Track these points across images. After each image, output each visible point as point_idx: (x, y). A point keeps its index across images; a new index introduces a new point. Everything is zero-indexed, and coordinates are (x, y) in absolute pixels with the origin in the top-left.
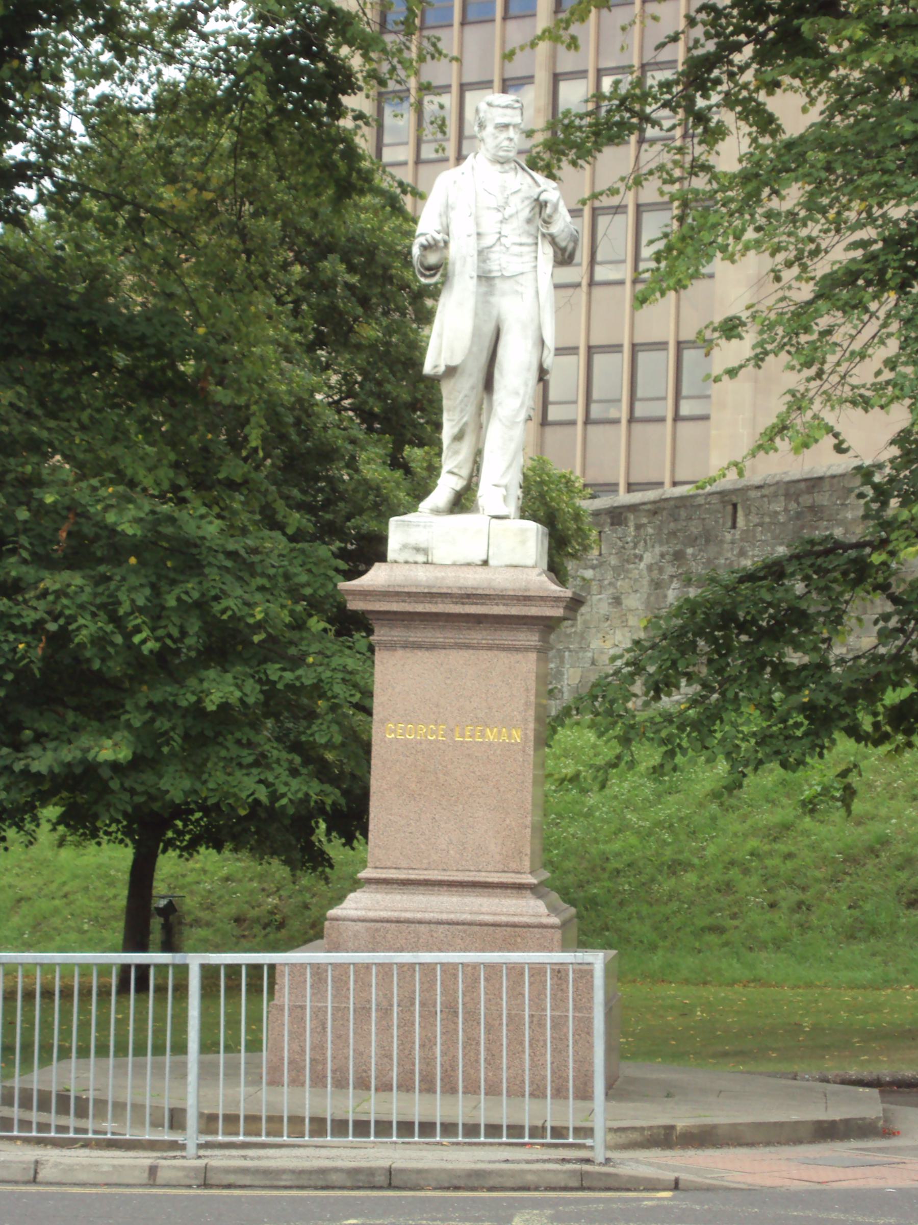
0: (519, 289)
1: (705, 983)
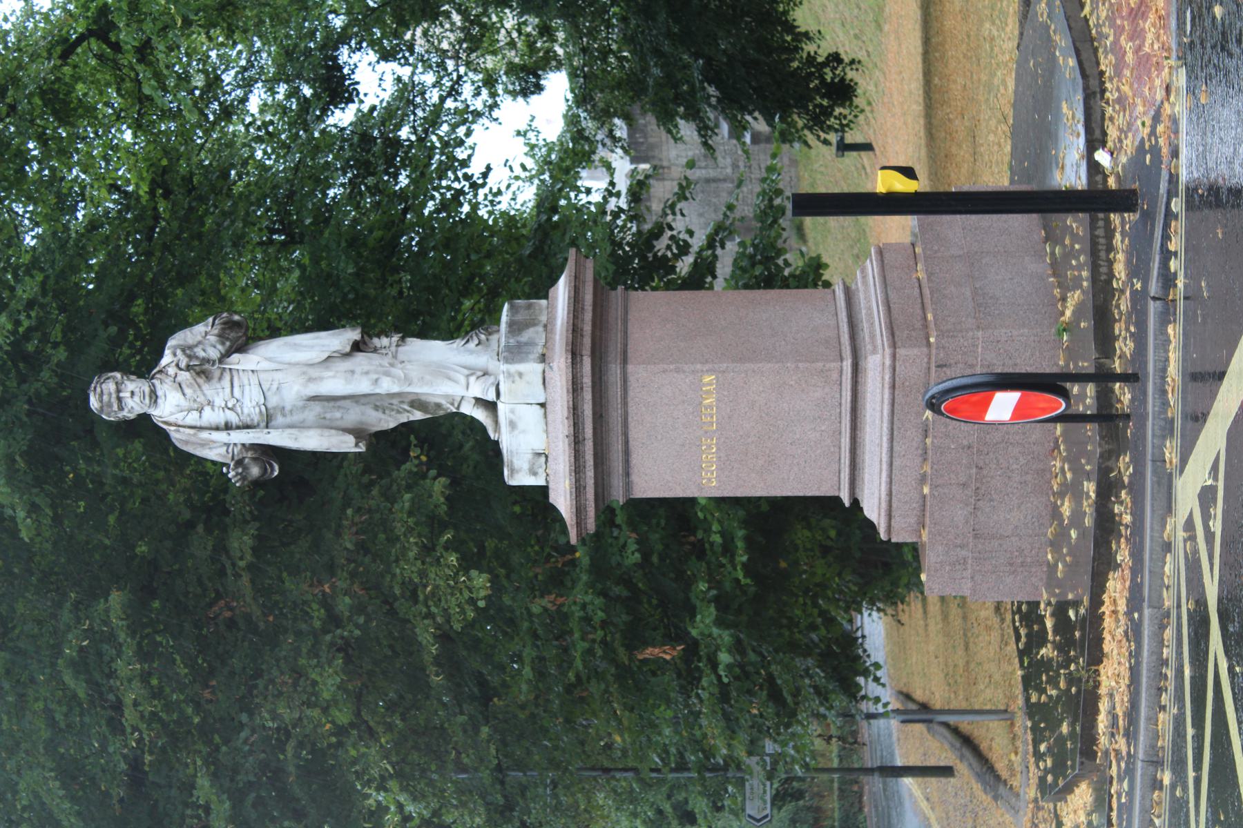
0: (275, 387)
1: (928, 799)
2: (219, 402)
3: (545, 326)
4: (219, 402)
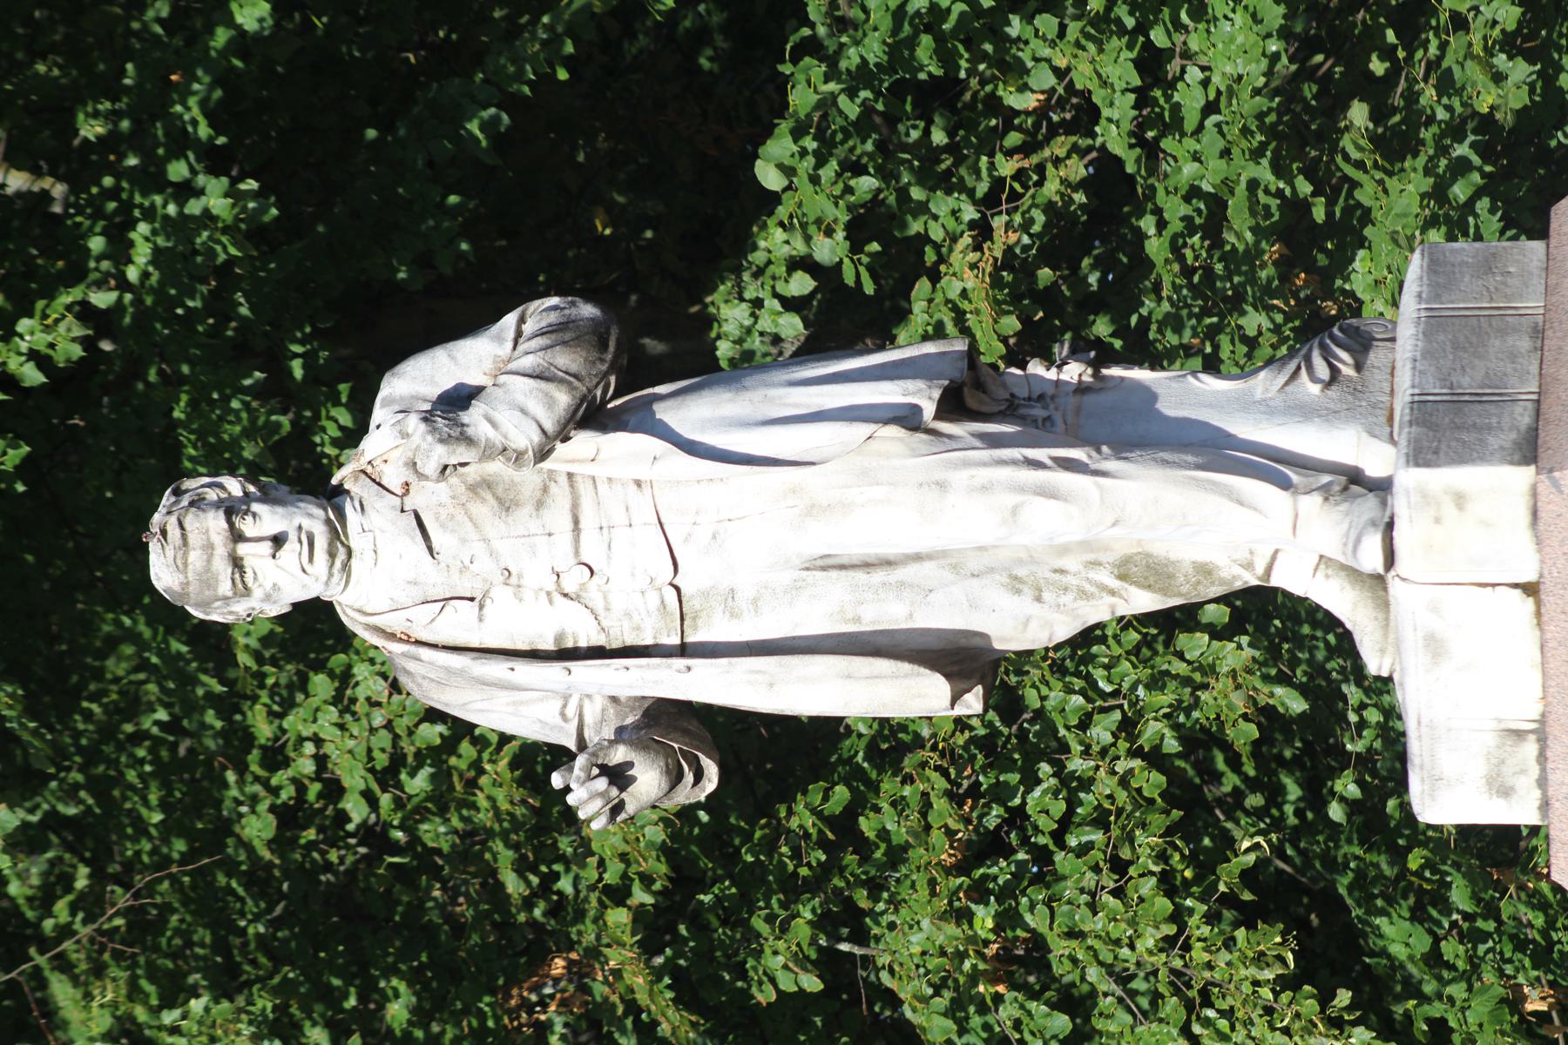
2: (537, 576)
3: (1538, 333)
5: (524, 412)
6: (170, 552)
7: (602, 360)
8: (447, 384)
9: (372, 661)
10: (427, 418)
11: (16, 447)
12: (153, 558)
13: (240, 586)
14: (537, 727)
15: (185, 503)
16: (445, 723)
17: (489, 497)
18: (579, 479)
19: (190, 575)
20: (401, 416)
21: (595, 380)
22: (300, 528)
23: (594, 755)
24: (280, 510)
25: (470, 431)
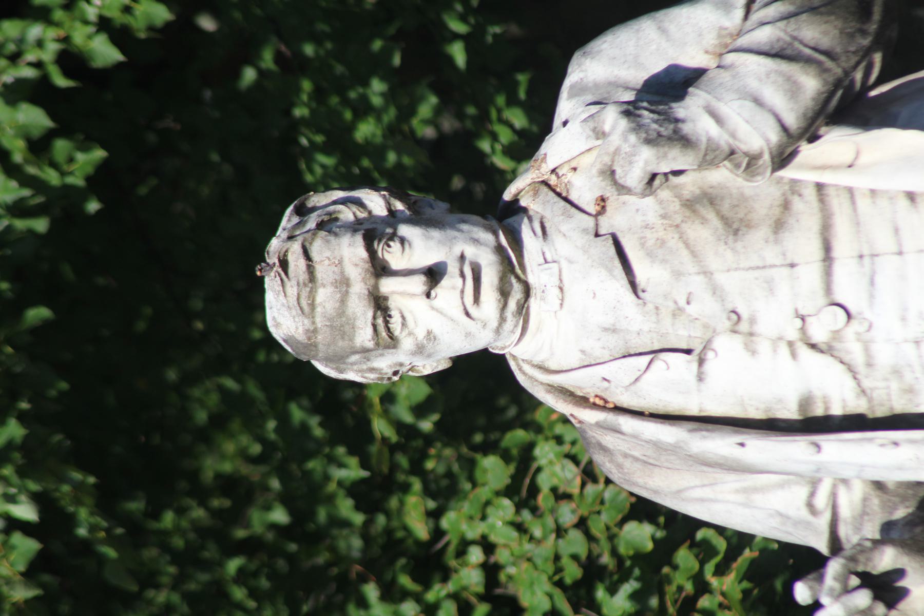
2: (774, 319)
4: (774, 319)
5: (758, 102)
6: (292, 290)
7: (863, 33)
8: (657, 66)
9: (559, 440)
10: (630, 111)
11: (84, 149)
12: (269, 297)
13: (384, 334)
14: (775, 522)
15: (311, 224)
16: (652, 520)
17: (711, 215)
18: (831, 192)
19: (319, 320)
20: (594, 109)
21: (854, 59)
22: (462, 257)
23: (852, 559)
24: (435, 233)
25: (686, 128)
